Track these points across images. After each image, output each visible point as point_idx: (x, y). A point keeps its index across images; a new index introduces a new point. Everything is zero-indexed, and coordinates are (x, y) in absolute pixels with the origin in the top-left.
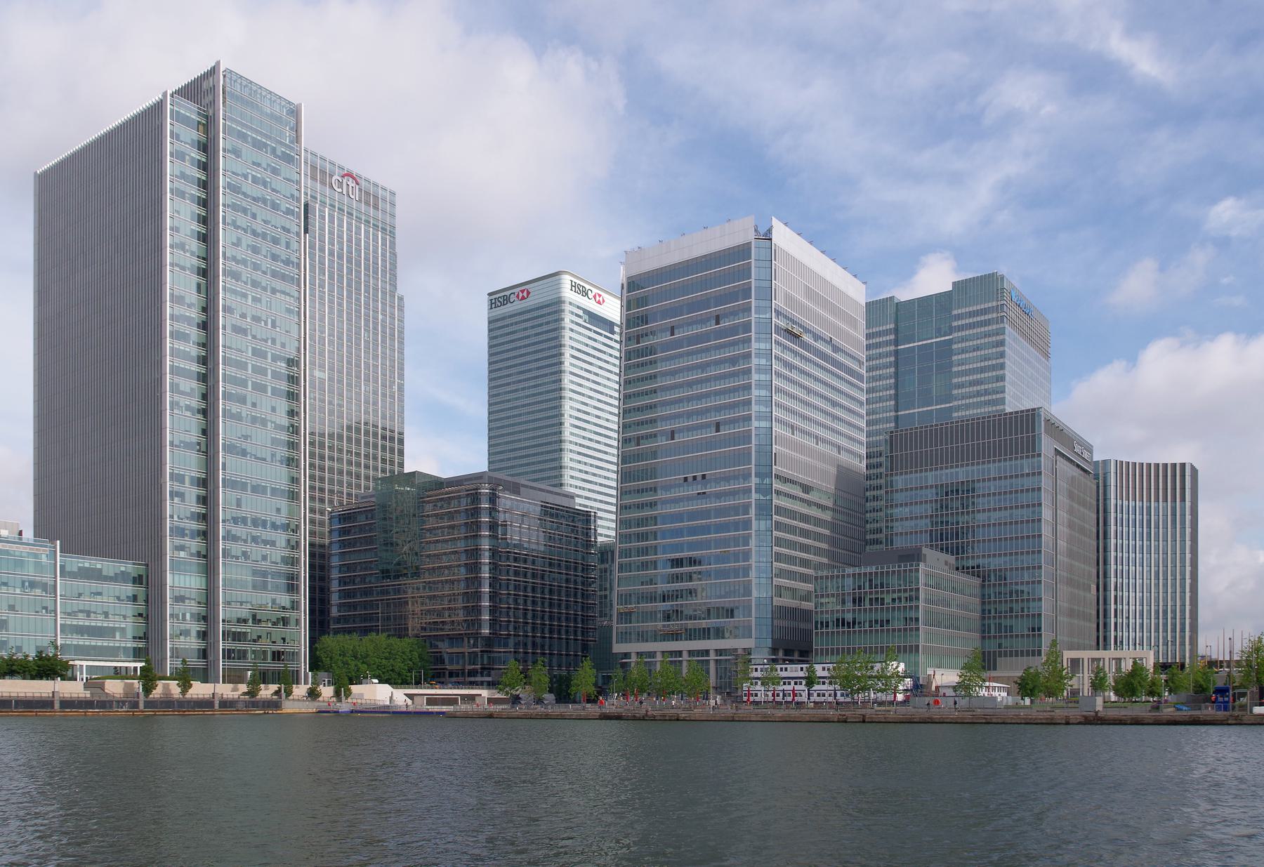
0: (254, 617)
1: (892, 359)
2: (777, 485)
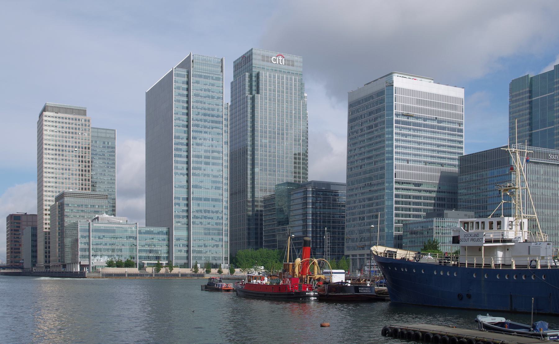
0: (205, 245)
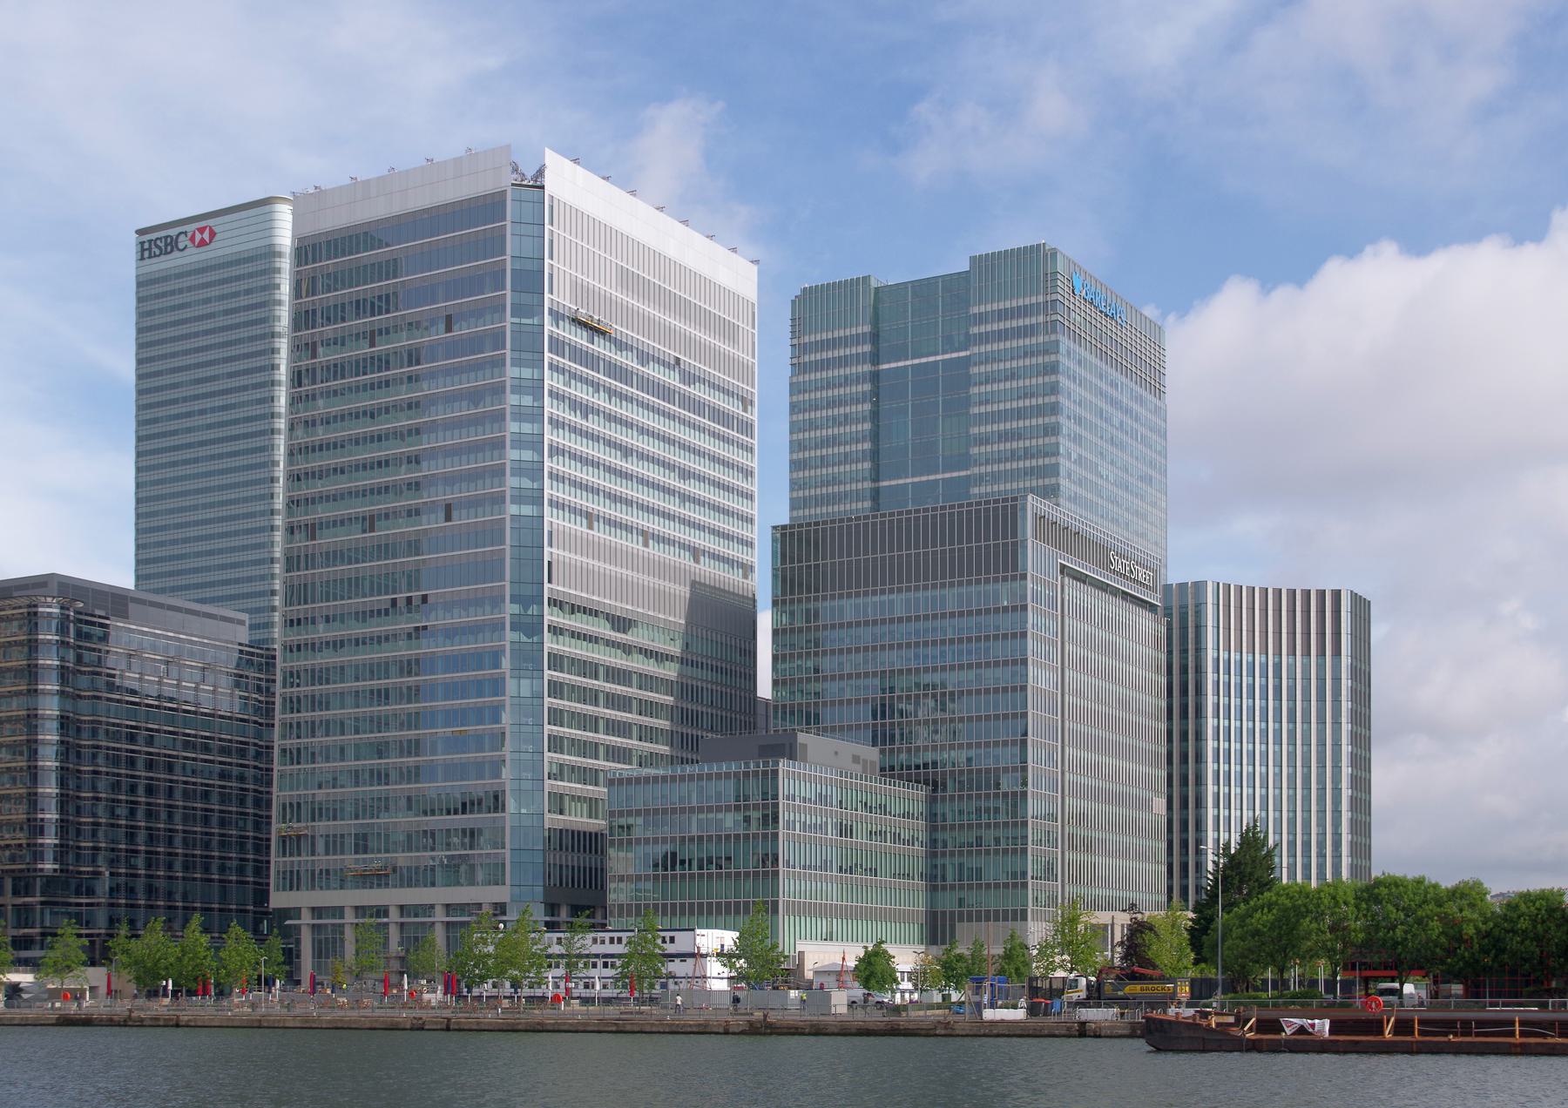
1: (867, 387)
2: (550, 616)
